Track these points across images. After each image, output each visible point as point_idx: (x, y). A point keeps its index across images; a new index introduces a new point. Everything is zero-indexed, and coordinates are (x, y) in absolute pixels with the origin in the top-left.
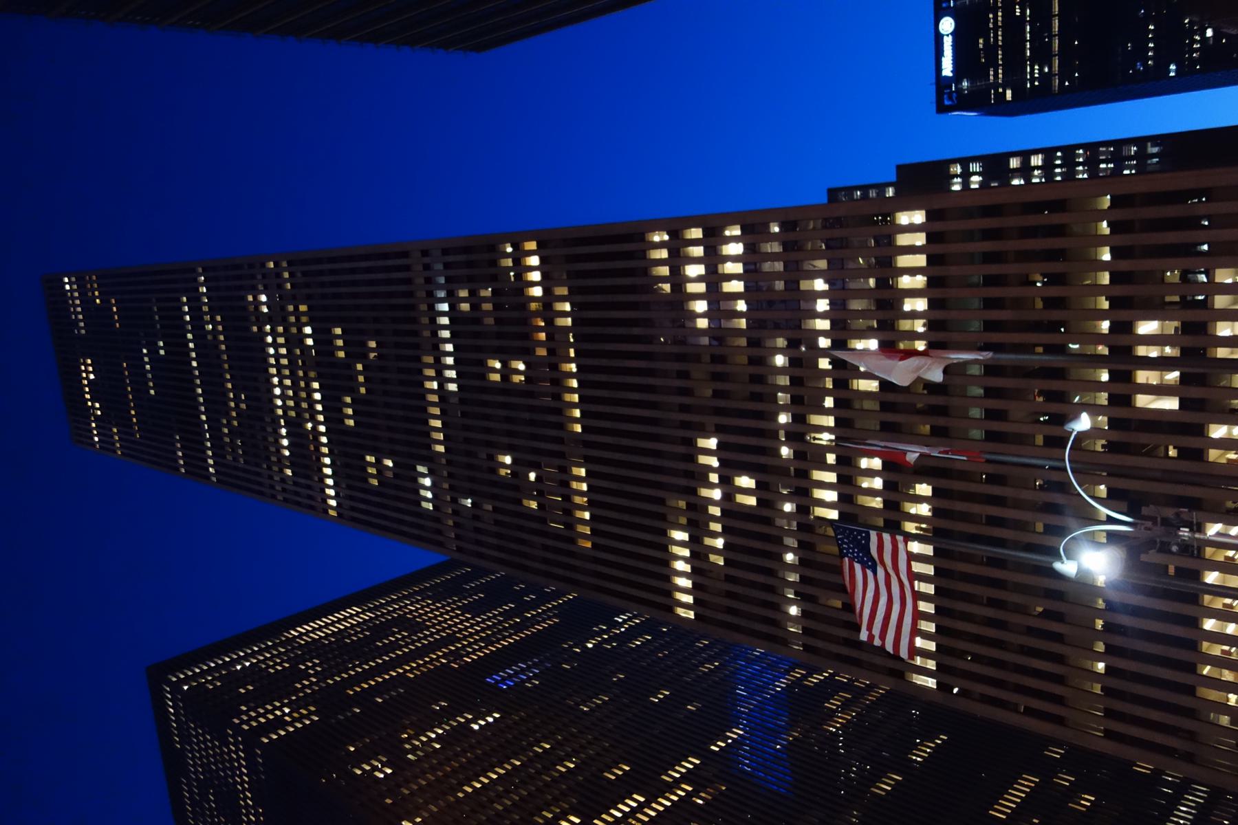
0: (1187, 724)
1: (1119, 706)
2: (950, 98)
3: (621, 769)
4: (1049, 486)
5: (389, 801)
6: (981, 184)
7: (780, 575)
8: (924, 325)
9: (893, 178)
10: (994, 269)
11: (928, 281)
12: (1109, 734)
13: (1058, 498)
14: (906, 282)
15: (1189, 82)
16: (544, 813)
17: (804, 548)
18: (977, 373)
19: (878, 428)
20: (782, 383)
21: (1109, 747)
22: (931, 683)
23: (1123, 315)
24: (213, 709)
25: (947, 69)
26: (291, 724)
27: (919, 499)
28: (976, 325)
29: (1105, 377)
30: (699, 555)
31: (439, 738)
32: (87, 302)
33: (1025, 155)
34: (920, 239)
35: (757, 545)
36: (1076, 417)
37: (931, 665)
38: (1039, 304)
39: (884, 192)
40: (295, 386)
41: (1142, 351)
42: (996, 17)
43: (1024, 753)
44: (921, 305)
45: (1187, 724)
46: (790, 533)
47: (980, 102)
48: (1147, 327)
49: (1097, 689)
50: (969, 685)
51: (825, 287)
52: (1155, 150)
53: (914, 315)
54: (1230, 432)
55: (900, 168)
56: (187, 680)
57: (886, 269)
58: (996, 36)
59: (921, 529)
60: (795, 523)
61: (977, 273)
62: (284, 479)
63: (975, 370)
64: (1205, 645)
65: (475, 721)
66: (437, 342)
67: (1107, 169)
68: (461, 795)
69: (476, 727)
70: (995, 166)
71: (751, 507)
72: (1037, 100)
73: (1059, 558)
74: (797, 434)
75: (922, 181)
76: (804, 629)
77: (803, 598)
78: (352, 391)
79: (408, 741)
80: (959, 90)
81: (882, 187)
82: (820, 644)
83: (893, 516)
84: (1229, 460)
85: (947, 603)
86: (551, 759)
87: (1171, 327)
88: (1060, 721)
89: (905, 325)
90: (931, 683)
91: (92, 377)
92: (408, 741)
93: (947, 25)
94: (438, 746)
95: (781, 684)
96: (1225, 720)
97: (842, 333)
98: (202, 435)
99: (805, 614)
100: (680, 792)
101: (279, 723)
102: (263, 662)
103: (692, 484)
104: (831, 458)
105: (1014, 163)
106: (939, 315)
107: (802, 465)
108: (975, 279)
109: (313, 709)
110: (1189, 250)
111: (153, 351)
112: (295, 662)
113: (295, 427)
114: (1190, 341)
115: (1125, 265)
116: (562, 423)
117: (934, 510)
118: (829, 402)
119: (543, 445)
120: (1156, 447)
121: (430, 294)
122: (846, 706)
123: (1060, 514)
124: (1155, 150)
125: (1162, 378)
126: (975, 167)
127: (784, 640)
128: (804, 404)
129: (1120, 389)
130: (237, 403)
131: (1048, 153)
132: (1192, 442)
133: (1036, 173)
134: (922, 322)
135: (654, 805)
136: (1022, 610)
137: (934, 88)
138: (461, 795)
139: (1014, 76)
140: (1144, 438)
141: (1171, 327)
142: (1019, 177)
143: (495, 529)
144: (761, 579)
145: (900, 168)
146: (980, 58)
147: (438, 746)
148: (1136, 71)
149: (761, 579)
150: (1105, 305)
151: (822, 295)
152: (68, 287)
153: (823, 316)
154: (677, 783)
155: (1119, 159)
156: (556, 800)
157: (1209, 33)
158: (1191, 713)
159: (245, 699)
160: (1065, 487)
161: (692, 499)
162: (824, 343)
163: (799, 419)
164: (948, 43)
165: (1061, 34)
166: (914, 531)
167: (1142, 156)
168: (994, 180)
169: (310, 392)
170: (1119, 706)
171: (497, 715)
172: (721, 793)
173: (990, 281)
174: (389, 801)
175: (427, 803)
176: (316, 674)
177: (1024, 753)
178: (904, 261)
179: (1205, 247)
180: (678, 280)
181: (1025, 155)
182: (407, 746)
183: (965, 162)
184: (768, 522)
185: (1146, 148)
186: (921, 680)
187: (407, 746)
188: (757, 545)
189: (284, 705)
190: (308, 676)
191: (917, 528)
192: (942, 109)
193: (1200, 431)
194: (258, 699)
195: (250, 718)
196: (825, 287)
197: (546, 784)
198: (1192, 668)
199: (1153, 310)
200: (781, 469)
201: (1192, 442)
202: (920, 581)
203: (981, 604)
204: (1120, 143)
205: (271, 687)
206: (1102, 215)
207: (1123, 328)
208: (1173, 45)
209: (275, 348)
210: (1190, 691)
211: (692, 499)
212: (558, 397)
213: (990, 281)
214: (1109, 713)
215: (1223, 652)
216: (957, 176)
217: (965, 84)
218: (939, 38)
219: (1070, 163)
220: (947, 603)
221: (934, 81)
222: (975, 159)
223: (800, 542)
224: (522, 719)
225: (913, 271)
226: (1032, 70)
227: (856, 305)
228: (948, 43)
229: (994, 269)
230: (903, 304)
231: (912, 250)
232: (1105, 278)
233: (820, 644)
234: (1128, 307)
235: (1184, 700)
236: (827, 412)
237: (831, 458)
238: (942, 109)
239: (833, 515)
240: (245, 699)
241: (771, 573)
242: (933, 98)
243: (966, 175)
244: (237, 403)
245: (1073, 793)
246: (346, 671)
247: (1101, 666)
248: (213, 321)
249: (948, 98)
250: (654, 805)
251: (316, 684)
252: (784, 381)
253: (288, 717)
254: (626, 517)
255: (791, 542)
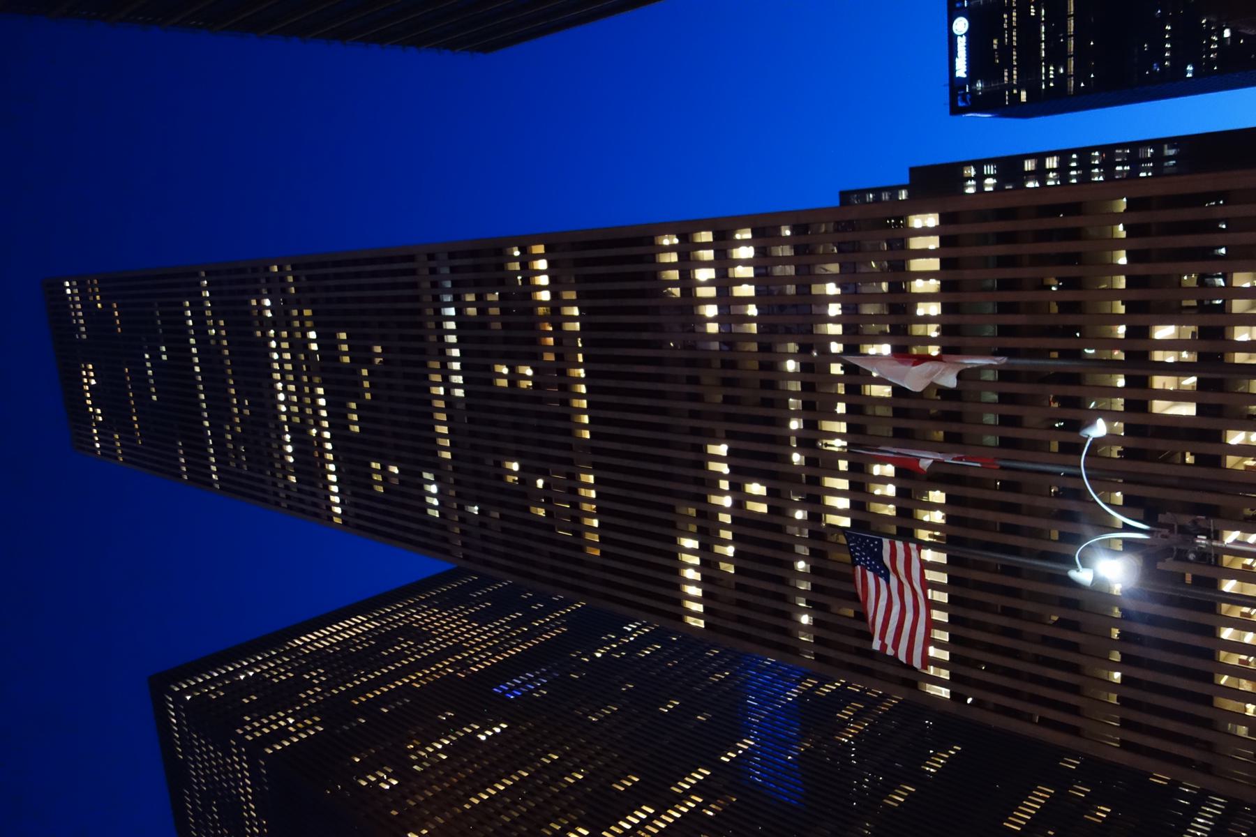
0: (1204, 734)
1: (1135, 716)
2: (964, 100)
3: (630, 780)
4: (1064, 493)
5: (394, 813)
6: (996, 186)
7: (792, 583)
8: (938, 330)
9: (906, 181)
10: (1008, 273)
11: (942, 285)
12: (1125, 745)
13: (1073, 505)
14: (919, 286)
15: (1206, 83)
16: (552, 825)
17: (815, 555)
18: (992, 378)
19: (891, 434)
20: (793, 389)
21: (1125, 758)
22: (945, 693)
23: (1140, 320)
24: (216, 720)
25: (961, 70)
26: (295, 734)
27: (933, 507)
28: (990, 330)
29: (1121, 382)
30: (709, 563)
31: (445, 749)
32: (88, 306)
33: (1040, 157)
34: (933, 243)
35: (768, 553)
36: (1091, 423)
37: (945, 674)
38: (1054, 309)
39: (897, 195)
40: (299, 392)
41: (1158, 356)
42: (1010, 17)
43: (1039, 764)
44: (934, 309)
45: (1204, 734)
46: (801, 541)
47: (994, 103)
48: (1163, 332)
49: (1113, 699)
50: (983, 695)
51: (837, 291)
52: (1172, 152)
53: (927, 320)
54: (1247, 438)
55: (913, 171)
56: (190, 690)
57: (899, 273)
58: (1010, 37)
59: (935, 537)
60: (806, 531)
61: (991, 277)
62: (288, 486)
63: (989, 376)
64: (1223, 654)
65: (482, 731)
66: (443, 347)
67: (1123, 171)
68: (467, 806)
69: (483, 738)
70: (1009, 168)
71: (762, 514)
72: (1052, 102)
73: (1075, 566)
74: (809, 441)
75: (935, 183)
76: (815, 638)
77: (814, 607)
78: (358, 397)
79: (414, 751)
80: (973, 92)
81: (894, 190)
82: (831, 653)
83: (906, 523)
84: (1247, 467)
85: (961, 612)
86: (559, 770)
87: (1188, 331)
88: (1075, 731)
89: (918, 330)
90: (945, 693)
91: (93, 382)
92: (414, 751)
93: (961, 25)
94: (444, 757)
95: (793, 694)
96: (1243, 731)
97: (854, 338)
98: (205, 441)
99: (816, 623)
100: (690, 804)
101: (283, 733)
102: (267, 671)
103: (702, 491)
104: (843, 465)
105: (1029, 165)
106: (953, 319)
107: (814, 472)
108: (989, 283)
109: (317, 719)
110: (1207, 254)
111: (156, 356)
112: (299, 671)
113: (299, 433)
114: (1207, 346)
115: (1141, 269)
116: (570, 429)
117: (948, 518)
118: (841, 408)
119: (551, 452)
120: (1173, 454)
121: (437, 298)
122: (858, 716)
123: (1075, 521)
124: (1172, 152)
125: (1179, 383)
126: (989, 169)
127: (795, 650)
128: (816, 410)
129: (1137, 394)
130: (240, 409)
131: (1064, 155)
132: (1209, 448)
133: (1051, 175)
134: (935, 326)
135: (663, 817)
136: (1037, 619)
137: (947, 89)
138: (467, 806)
139: (1029, 77)
140: (1161, 444)
141: (1188, 331)
142: (1034, 180)
143: (502, 536)
144: (772, 587)
145: (913, 171)
146: (994, 59)
147: (444, 757)
148: (1153, 72)
149: (772, 587)
150: (1121, 309)
151: (834, 299)
152: (69, 291)
153: (835, 320)
154: (686, 794)
155: (1135, 162)
156: (564, 812)
157: (1227, 33)
158: (1208, 724)
159: (249, 709)
160: (1081, 494)
161: (702, 507)
162: (836, 348)
163: (811, 425)
164: (962, 43)
165: (1076, 35)
166: (927, 539)
167: (1158, 158)
168: (1009, 182)
169: (315, 397)
170: (1135, 716)
171: (504, 726)
172: (732, 804)
173: (1005, 285)
174: (394, 813)
175: (433, 815)
176: (321, 684)
177: (1039, 764)
178: (917, 265)
179: (1223, 251)
180: (688, 284)
181: (1040, 157)
182: (413, 757)
183: (979, 164)
184: (780, 529)
185: (1162, 150)
186: (934, 690)
187: (413, 757)
188: (768, 553)
189: (288, 715)
190: (312, 686)
191: (930, 536)
192: (955, 110)
193: (1217, 437)
194: (262, 709)
195: (253, 728)
196: (837, 291)
197: (554, 796)
198: (1209, 678)
199: (1170, 314)
200: (792, 476)
201: (1209, 448)
202: (933, 589)
203: (995, 613)
204: (1137, 146)
205: (275, 697)
206: (1118, 218)
207: (1139, 333)
208: (1190, 45)
209: (279, 353)
210: (1208, 701)
211: (702, 507)
212: (566, 403)
213: (1005, 285)
214: (1125, 724)
215: (1241, 661)
216: (970, 178)
217: (979, 85)
218: (952, 39)
219: (1085, 165)
220: (961, 612)
221: (947, 82)
222: (989, 161)
223: (811, 550)
224: (529, 729)
225: (926, 275)
226: (1047, 71)
227: (869, 309)
228: (962, 43)
229: (1008, 273)
230: (916, 308)
231: (925, 253)
232: (1121, 283)
233: (831, 653)
234: (1144, 311)
235: (1201, 711)
236: (839, 418)
237: (843, 465)
238: (955, 110)
239: (845, 522)
240: (249, 709)
241: (782, 581)
242: (947, 100)
243: (980, 178)
244: (240, 409)
245: (1089, 804)
246: (351, 680)
247: (1117, 676)
248: (216, 326)
249: (961, 99)
250: (663, 817)
251: (320, 694)
252: (795, 386)
253: (292, 727)
254: (635, 525)
255: (803, 550)
